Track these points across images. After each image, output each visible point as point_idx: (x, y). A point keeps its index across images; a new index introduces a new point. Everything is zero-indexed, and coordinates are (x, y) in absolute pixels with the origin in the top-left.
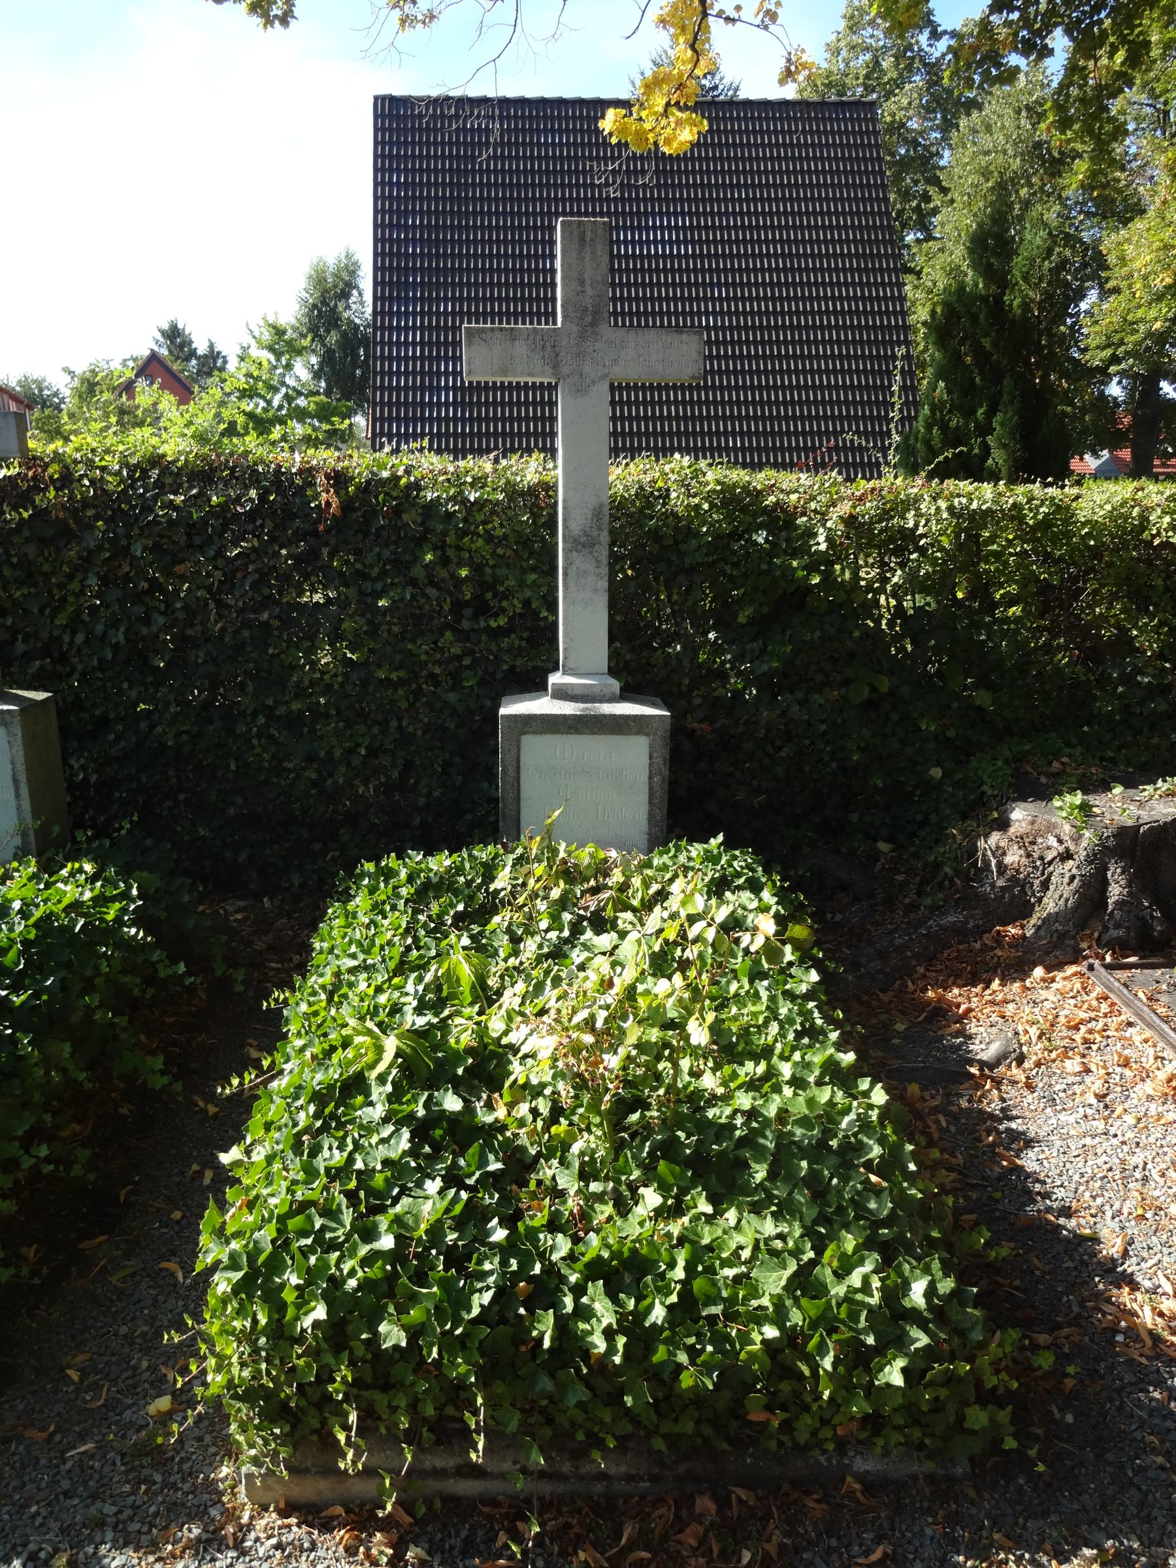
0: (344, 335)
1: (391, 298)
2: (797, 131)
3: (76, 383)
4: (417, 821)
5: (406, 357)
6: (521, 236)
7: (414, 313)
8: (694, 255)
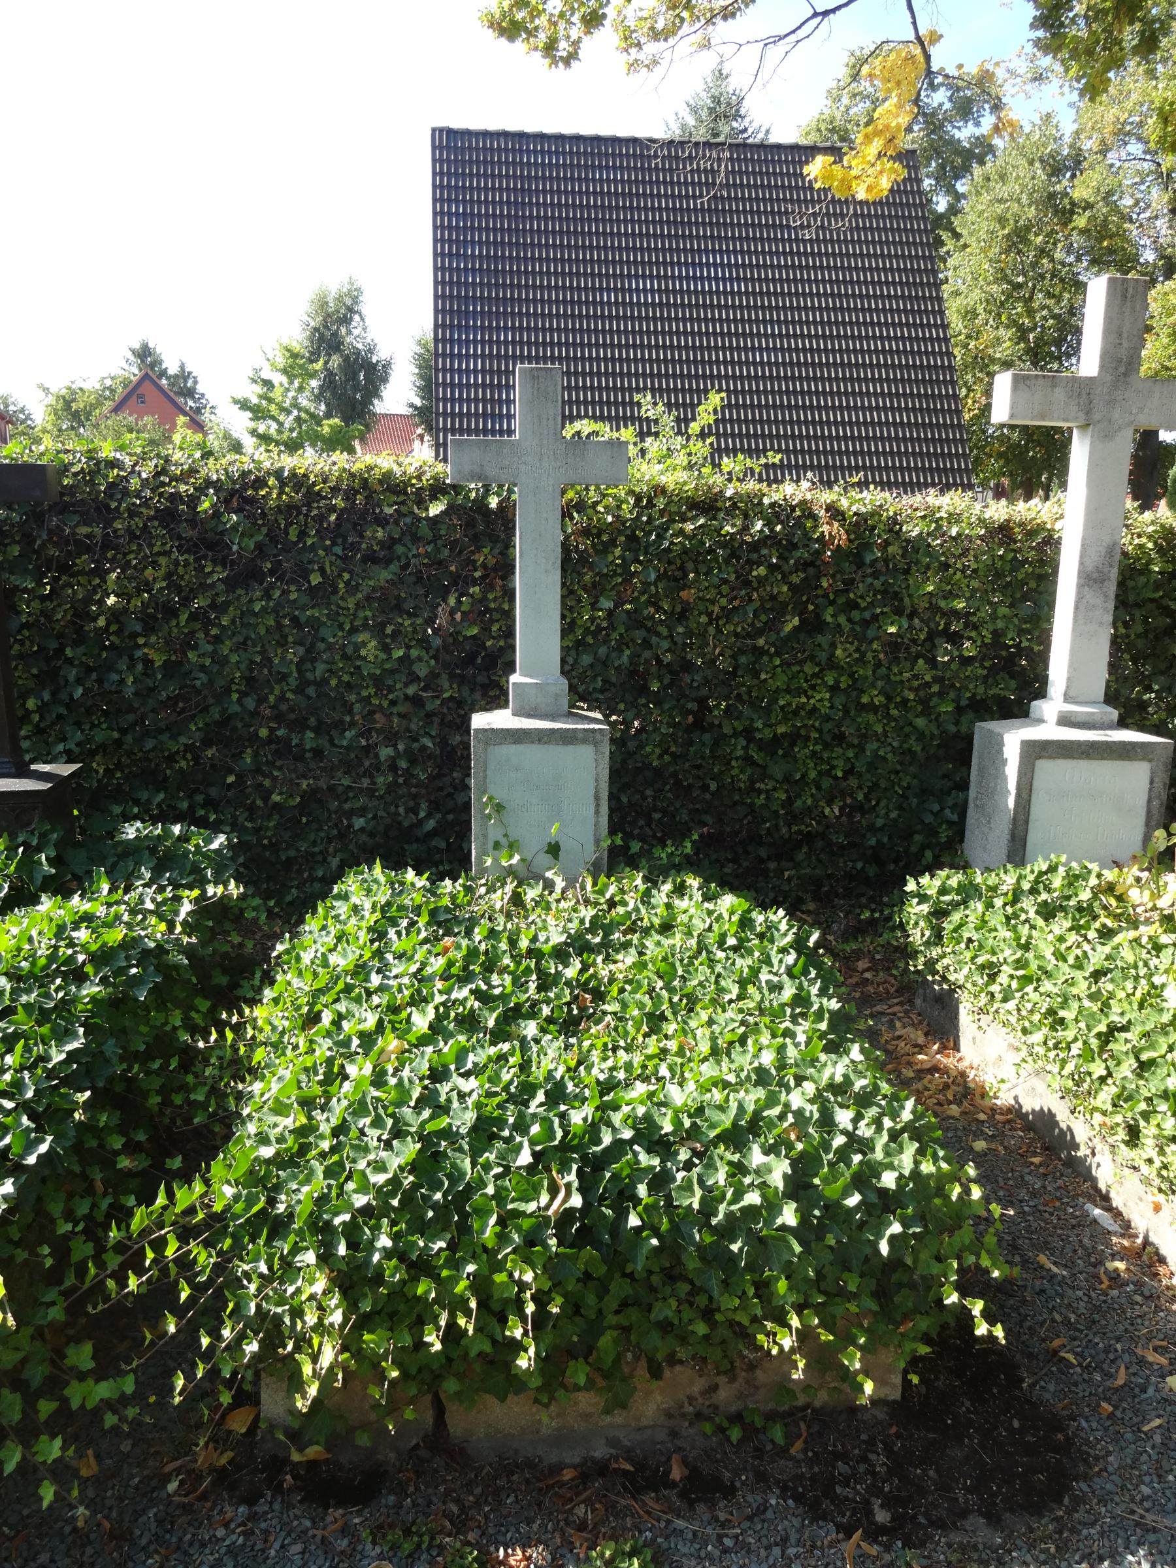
0: (346, 359)
1: (452, 326)
2: (678, 169)
3: (51, 400)
4: (873, 842)
5: (468, 385)
7: (475, 341)
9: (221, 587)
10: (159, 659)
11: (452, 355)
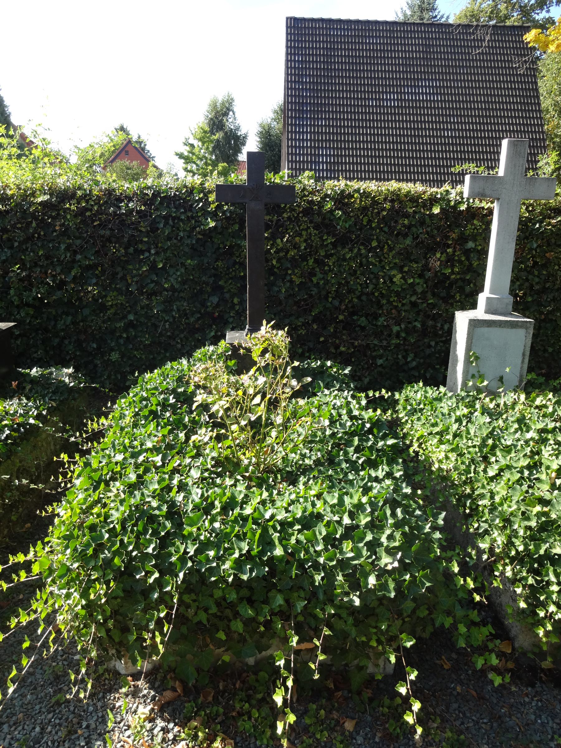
0: (226, 133)
6: (357, 88)
7: (307, 125)
8: (441, 101)
9: (330, 246)
10: (297, 281)
11: (295, 132)
